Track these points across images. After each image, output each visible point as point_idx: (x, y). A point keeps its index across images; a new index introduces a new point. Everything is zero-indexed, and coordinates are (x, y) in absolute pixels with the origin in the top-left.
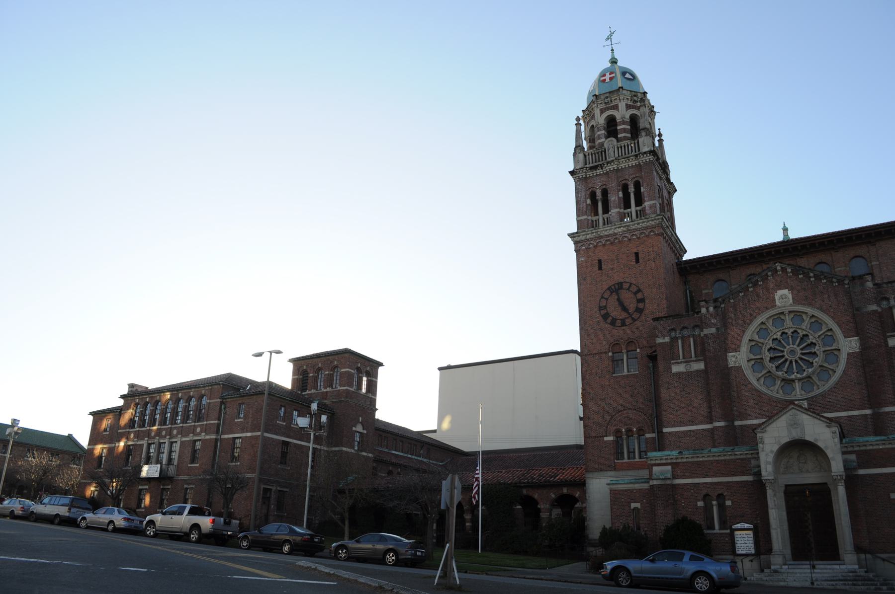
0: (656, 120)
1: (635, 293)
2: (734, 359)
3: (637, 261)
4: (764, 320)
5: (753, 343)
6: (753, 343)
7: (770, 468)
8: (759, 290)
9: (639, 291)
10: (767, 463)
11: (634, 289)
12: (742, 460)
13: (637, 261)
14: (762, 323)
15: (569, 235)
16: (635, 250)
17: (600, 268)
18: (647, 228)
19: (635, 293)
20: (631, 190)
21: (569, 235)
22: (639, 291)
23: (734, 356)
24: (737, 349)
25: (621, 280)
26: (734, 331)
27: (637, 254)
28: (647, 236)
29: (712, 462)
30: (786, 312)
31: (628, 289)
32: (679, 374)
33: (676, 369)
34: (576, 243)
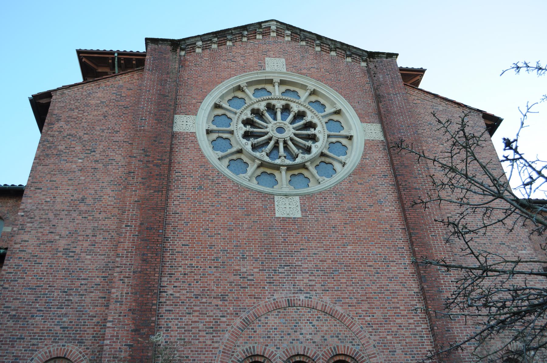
5: (214, 136)
6: (219, 112)
14: (239, 88)
24: (193, 111)
30: (277, 80)
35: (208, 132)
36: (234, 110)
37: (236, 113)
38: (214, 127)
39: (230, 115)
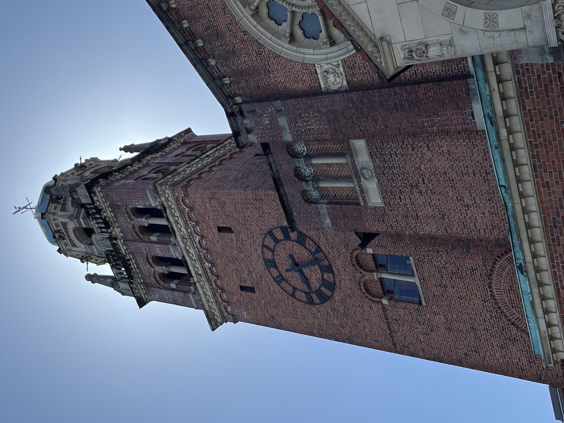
0: (161, 138)
1: (277, 241)
2: (331, 78)
3: (228, 230)
4: (247, 13)
5: (299, 32)
6: (299, 32)
7: (508, 18)
8: (199, 28)
9: (270, 233)
10: (491, 25)
11: (269, 242)
12: (522, 94)
13: (228, 230)
15: (213, 329)
16: (215, 230)
17: (252, 290)
18: (182, 212)
19: (277, 241)
20: (145, 222)
21: (213, 329)
22: (270, 233)
23: (326, 79)
24: (310, 69)
25: (261, 261)
26: (279, 79)
27: (220, 229)
28: (191, 209)
29: (542, 187)
31: (273, 251)
32: (383, 192)
33: (375, 198)
34: (225, 320)
35: (332, 42)
36: (289, 14)
37: (293, 13)
38: (323, 34)
39: (298, 18)
